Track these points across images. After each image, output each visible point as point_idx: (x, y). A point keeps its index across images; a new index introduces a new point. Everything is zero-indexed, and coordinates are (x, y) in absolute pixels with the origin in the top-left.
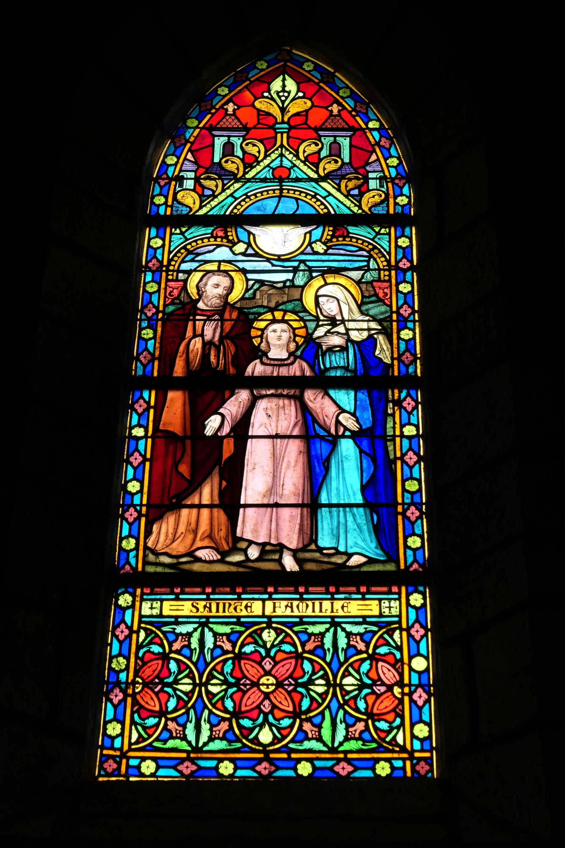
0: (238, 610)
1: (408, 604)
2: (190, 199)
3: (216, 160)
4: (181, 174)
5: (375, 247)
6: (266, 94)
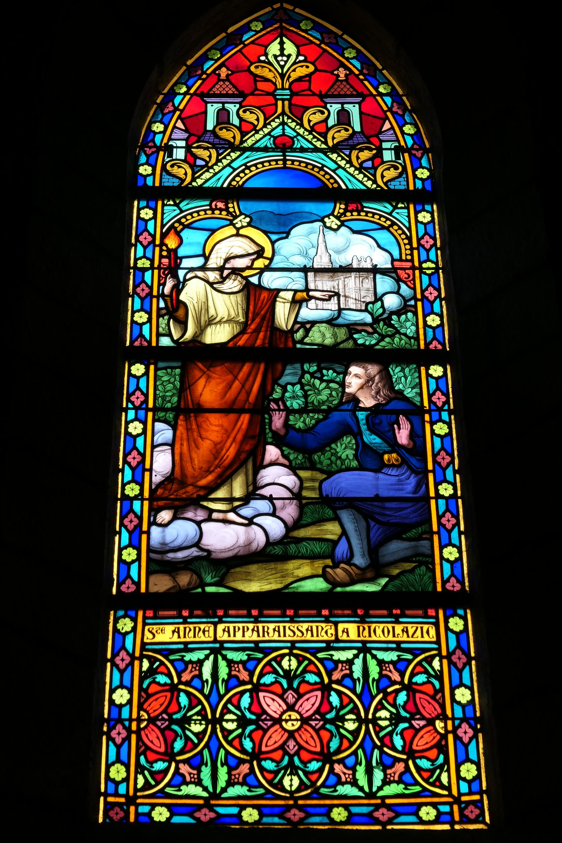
2: (183, 171)
3: (210, 126)
4: (170, 143)
5: (393, 224)
6: (263, 58)
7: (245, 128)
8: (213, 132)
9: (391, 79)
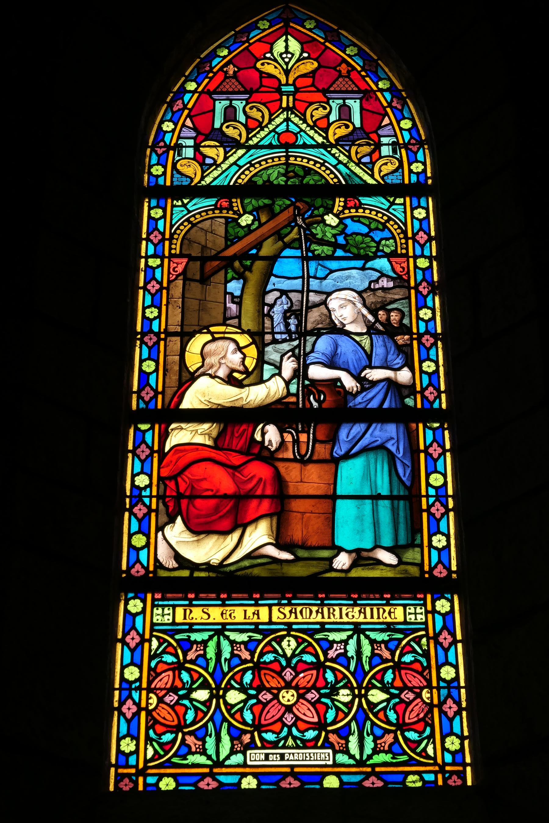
2: (192, 170)
3: (217, 125)
4: (179, 142)
5: (390, 219)
6: (268, 55)
7: (251, 124)
9: (390, 75)
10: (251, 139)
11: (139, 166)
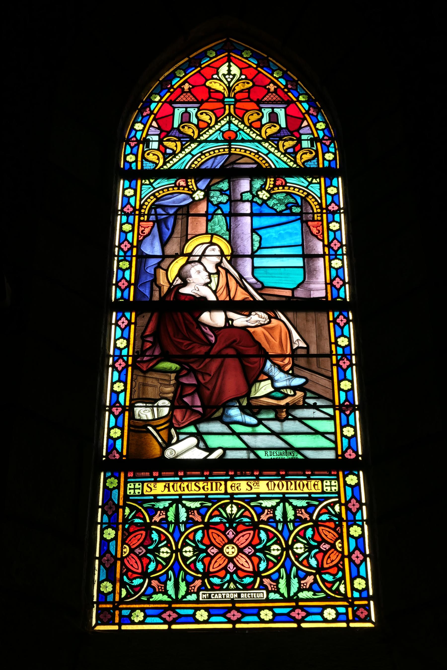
0: (206, 489)
1: (345, 484)
3: (176, 125)
4: (147, 138)
5: (309, 194)
6: (215, 76)
7: (202, 125)
8: (178, 129)
10: (202, 135)
11: (116, 155)
